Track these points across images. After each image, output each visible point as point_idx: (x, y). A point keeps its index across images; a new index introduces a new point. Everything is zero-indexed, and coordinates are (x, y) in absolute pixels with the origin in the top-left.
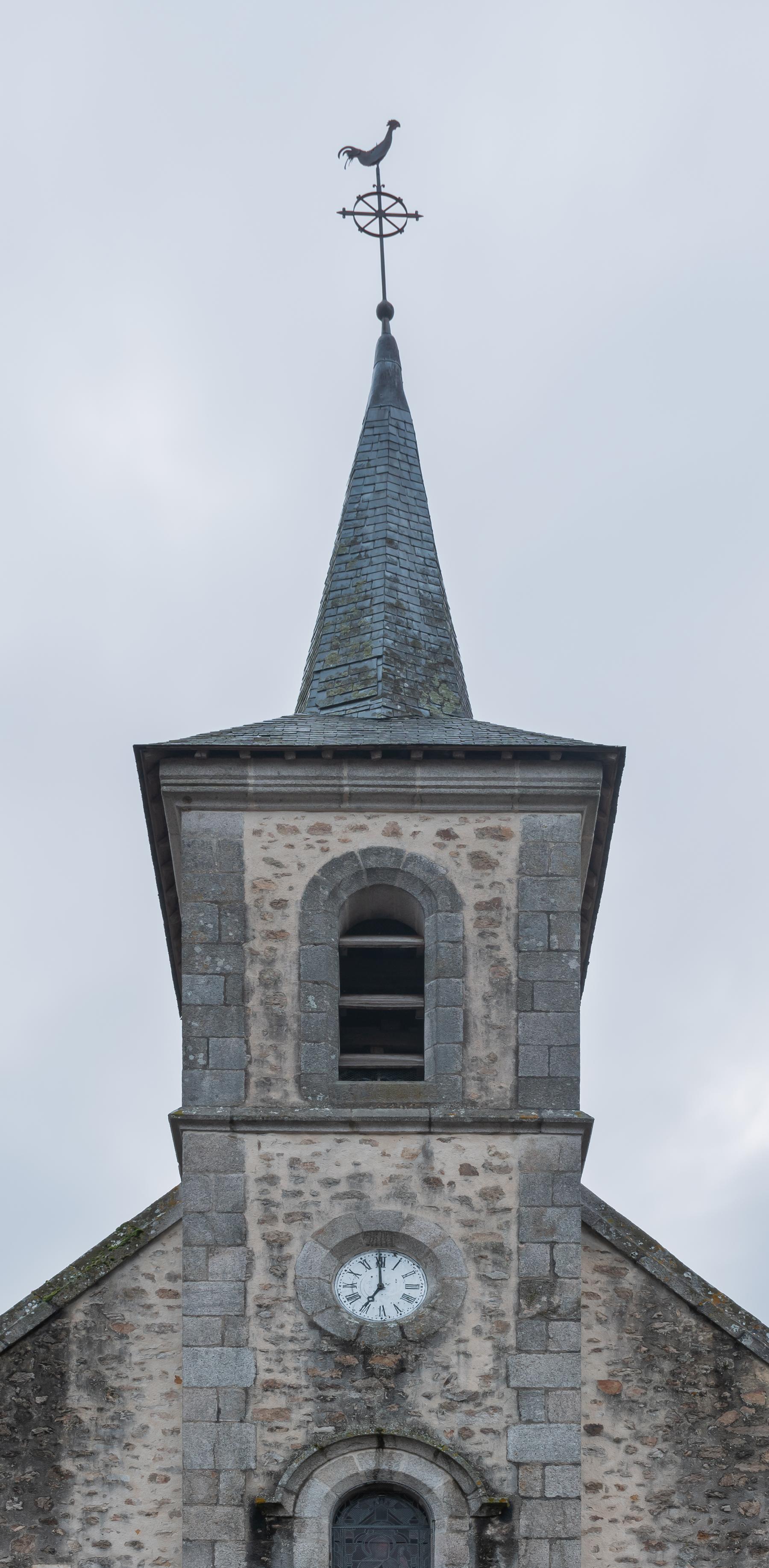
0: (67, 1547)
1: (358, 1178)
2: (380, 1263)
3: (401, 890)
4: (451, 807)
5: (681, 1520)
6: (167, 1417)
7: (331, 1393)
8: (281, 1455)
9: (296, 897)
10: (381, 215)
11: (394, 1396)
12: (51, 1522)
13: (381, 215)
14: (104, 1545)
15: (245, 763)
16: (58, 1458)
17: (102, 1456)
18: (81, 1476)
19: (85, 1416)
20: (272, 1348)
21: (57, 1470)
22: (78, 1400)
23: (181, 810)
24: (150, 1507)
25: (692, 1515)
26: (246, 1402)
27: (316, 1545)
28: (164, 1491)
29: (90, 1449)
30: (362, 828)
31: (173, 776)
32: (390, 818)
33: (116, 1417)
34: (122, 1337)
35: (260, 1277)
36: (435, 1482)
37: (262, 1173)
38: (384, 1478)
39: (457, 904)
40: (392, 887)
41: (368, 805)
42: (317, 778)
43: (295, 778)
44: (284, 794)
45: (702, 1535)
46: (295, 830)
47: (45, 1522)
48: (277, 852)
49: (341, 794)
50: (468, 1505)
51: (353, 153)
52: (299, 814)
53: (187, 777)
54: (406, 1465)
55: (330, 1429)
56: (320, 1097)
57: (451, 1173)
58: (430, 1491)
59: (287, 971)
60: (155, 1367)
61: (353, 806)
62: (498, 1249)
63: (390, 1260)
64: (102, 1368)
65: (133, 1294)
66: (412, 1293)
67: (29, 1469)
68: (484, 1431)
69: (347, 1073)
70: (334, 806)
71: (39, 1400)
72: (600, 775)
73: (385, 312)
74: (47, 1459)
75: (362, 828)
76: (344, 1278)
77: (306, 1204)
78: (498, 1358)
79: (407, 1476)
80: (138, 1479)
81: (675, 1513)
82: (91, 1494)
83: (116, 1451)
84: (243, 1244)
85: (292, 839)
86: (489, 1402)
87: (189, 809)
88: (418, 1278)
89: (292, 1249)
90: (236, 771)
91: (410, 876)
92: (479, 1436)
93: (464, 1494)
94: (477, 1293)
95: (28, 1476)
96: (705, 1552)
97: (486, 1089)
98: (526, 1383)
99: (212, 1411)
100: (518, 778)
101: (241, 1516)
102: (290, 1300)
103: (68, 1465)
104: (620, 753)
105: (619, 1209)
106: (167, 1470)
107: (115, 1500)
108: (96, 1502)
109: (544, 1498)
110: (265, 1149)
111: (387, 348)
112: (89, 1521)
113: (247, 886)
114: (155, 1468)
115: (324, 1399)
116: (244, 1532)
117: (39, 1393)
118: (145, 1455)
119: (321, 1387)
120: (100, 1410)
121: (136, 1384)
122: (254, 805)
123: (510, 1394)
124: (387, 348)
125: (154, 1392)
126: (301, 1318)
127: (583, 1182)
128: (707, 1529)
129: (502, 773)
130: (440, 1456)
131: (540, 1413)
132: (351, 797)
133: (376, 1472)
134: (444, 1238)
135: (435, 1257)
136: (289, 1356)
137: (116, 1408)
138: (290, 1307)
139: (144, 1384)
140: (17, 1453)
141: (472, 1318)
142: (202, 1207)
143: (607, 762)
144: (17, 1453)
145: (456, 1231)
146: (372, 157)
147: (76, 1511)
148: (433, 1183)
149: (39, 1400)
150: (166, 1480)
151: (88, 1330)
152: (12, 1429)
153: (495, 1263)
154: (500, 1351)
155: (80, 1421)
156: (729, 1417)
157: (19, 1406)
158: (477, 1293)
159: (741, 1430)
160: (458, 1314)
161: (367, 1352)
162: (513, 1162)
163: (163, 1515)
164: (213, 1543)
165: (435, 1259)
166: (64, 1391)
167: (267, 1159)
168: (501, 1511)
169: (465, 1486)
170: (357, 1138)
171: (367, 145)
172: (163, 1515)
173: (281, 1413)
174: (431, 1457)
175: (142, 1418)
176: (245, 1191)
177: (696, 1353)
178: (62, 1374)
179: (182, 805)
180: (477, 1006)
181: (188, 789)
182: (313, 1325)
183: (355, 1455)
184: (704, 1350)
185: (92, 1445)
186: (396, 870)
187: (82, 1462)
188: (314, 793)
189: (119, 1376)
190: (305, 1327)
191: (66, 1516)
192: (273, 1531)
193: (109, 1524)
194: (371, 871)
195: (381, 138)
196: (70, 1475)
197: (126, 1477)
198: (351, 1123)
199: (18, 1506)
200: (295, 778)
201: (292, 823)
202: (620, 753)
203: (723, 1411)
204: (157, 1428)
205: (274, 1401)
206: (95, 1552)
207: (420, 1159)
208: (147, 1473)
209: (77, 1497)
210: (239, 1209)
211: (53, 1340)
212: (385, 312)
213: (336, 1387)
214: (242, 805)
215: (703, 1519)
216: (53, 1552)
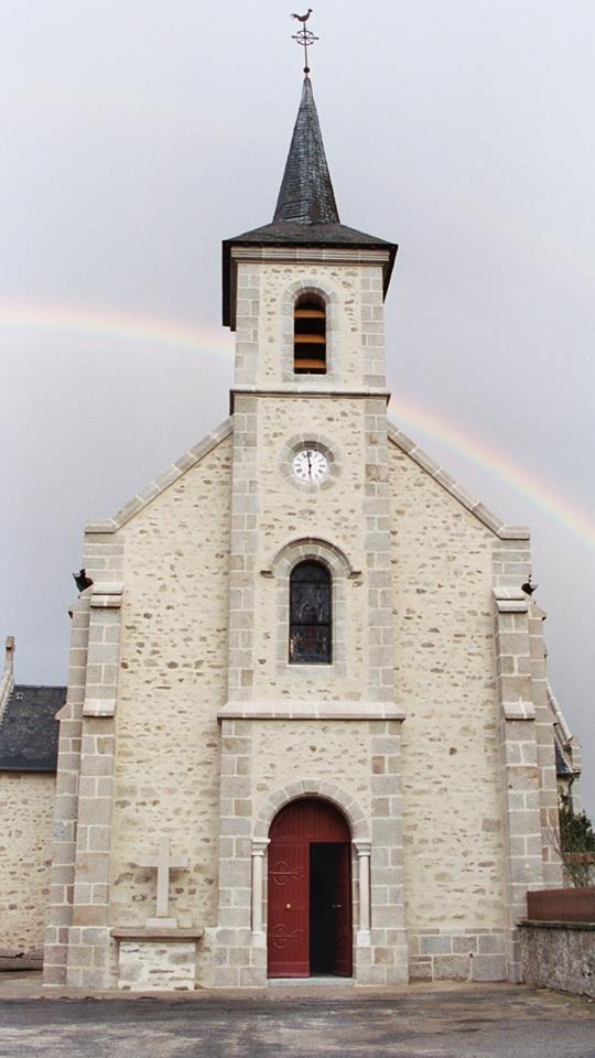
2: (309, 455)
10: (305, 38)
13: (305, 38)
15: (261, 247)
24: (216, 570)
27: (17, 885)
30: (302, 271)
31: (236, 252)
32: (314, 267)
46: (279, 272)
48: (272, 281)
51: (296, 16)
63: (314, 453)
66: (322, 469)
69: (298, 371)
72: (388, 253)
75: (302, 271)
76: (296, 462)
85: (277, 274)
88: (324, 462)
98: (191, 778)
100: (360, 255)
104: (396, 246)
105: (337, 203)
110: (266, 404)
111: (307, 82)
124: (307, 82)
127: (270, 222)
132: (300, 260)
143: (392, 249)
146: (303, 19)
171: (301, 15)
195: (306, 14)
202: (396, 246)
212: (307, 70)
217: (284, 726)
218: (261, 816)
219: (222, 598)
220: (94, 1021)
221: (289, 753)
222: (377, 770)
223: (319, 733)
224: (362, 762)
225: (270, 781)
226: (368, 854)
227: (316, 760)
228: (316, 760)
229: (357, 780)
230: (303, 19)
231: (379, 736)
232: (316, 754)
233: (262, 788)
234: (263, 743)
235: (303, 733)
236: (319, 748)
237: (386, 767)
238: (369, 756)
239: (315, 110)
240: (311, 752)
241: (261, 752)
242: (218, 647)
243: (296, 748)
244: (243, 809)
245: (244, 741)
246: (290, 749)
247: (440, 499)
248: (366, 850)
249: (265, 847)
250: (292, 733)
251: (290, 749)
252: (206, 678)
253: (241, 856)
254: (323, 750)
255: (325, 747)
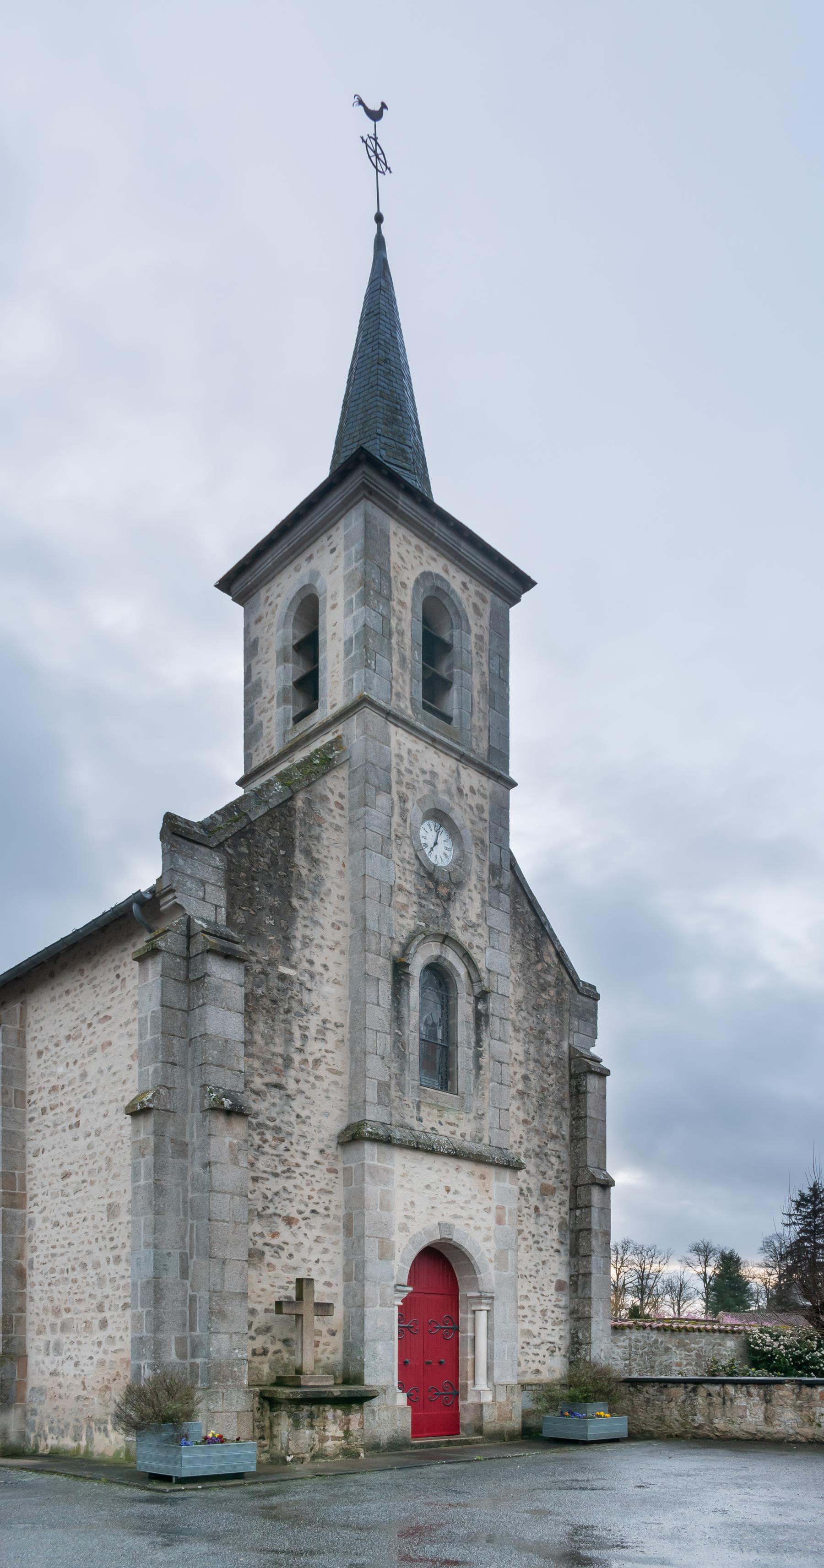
0: (294, 958)
1: (434, 774)
3: (444, 606)
4: (469, 571)
5: (524, 1018)
6: (339, 887)
7: (424, 902)
8: (405, 934)
9: (411, 584)
11: (446, 914)
12: (287, 939)
14: (311, 962)
16: (290, 896)
17: (310, 902)
18: (302, 913)
19: (304, 872)
20: (399, 862)
21: (290, 903)
22: (299, 858)
23: (365, 496)
25: (528, 1016)
26: (391, 895)
28: (338, 935)
29: (305, 896)
33: (316, 878)
34: (320, 826)
35: (396, 819)
36: (461, 969)
37: (397, 752)
38: (440, 961)
39: (469, 631)
40: (441, 602)
41: (439, 548)
42: (425, 519)
43: (417, 513)
44: (411, 519)
45: (531, 1029)
47: (284, 937)
49: (433, 535)
50: (473, 989)
52: (412, 535)
53: (374, 480)
54: (452, 957)
55: (423, 924)
56: (420, 716)
57: (466, 790)
58: (459, 975)
59: (406, 626)
60: (334, 852)
61: (434, 544)
62: (482, 842)
64: (311, 843)
65: (324, 799)
66: (448, 853)
67: (277, 899)
68: (478, 947)
70: (426, 539)
71: (282, 852)
73: (379, 219)
74: (285, 893)
77: (413, 780)
78: (482, 906)
79: (450, 963)
80: (326, 922)
81: (524, 1014)
82: (306, 926)
83: (317, 901)
84: (390, 793)
86: (480, 930)
87: (368, 499)
89: (409, 805)
90: (395, 492)
91: (451, 601)
92: (475, 948)
93: (472, 981)
94: (475, 865)
95: (276, 903)
96: (532, 1038)
97: (478, 745)
99: (377, 895)
101: (389, 965)
102: (408, 837)
103: (295, 902)
106: (340, 922)
107: (315, 933)
108: (308, 932)
109: (497, 993)
111: (380, 243)
112: (305, 945)
113: (392, 565)
114: (335, 918)
115: (421, 905)
116: (390, 977)
117: (282, 847)
118: (330, 909)
119: (420, 897)
120: (310, 870)
121: (325, 860)
122: (396, 516)
123: (487, 929)
124: (380, 243)
125: (334, 867)
126: (412, 852)
128: (532, 1026)
129: (491, 565)
130: (467, 957)
131: (497, 944)
133: (440, 956)
134: (465, 827)
135: (461, 836)
136: (407, 873)
137: (316, 872)
138: (408, 841)
139: (329, 861)
140: (271, 886)
141: (474, 879)
142: (374, 761)
144: (271, 886)
145: (468, 824)
147: (298, 934)
148: (460, 791)
149: (282, 852)
150: (339, 929)
151: (304, 814)
152: (269, 867)
153: (482, 850)
154: (483, 902)
155: (301, 875)
156: (539, 967)
157: (272, 852)
158: (475, 865)
159: (543, 975)
160: (469, 875)
161: (437, 883)
162: (488, 793)
163: (337, 951)
164: (379, 979)
165: (461, 837)
166: (293, 851)
167: (399, 744)
168: (483, 996)
169: (473, 978)
170: (433, 750)
172: (337, 951)
173: (405, 907)
174: (461, 956)
175: (328, 884)
176: (391, 761)
177: (529, 927)
178: (293, 839)
179: (367, 495)
180: (475, 694)
181: (375, 488)
182: (417, 857)
183: (433, 944)
184: (532, 926)
185: (307, 894)
186: (447, 594)
187: (301, 902)
188: (423, 527)
189: (318, 851)
190: (413, 857)
191: (295, 937)
192: (401, 980)
193: (314, 949)
194: (438, 588)
196: (294, 910)
197: (321, 921)
198: (434, 740)
199: (272, 922)
200: (417, 513)
201: (409, 538)
203: (538, 962)
204: (336, 892)
205: (401, 898)
206: (307, 965)
207: (456, 775)
208: (331, 922)
209: (299, 926)
210: (388, 770)
211: (288, 813)
212: (379, 219)
213: (424, 898)
214: (391, 512)
215: (531, 1019)
216: (288, 960)
217: (423, 1159)
218: (403, 1261)
219: (338, 983)
220: (465, 1350)
221: (427, 1191)
222: (499, 1221)
223: (452, 1171)
224: (487, 1210)
225: (410, 1221)
226: (488, 1308)
227: (449, 1203)
228: (449, 1203)
229: (483, 1229)
230: (375, 116)
231: (502, 1184)
232: (450, 1197)
233: (404, 1228)
234: (404, 1175)
235: (439, 1170)
236: (452, 1190)
237: (507, 1218)
238: (493, 1204)
239: (360, 327)
240: (445, 1193)
241: (402, 1186)
242: (337, 1047)
243: (433, 1186)
244: (386, 1253)
245: (387, 1171)
246: (428, 1187)
247: (327, 1081)
248: (487, 1304)
249: (405, 1295)
250: (429, 1169)
251: (428, 1187)
252: (324, 1085)
253: (386, 1306)
254: (456, 1192)
255: (458, 1189)
